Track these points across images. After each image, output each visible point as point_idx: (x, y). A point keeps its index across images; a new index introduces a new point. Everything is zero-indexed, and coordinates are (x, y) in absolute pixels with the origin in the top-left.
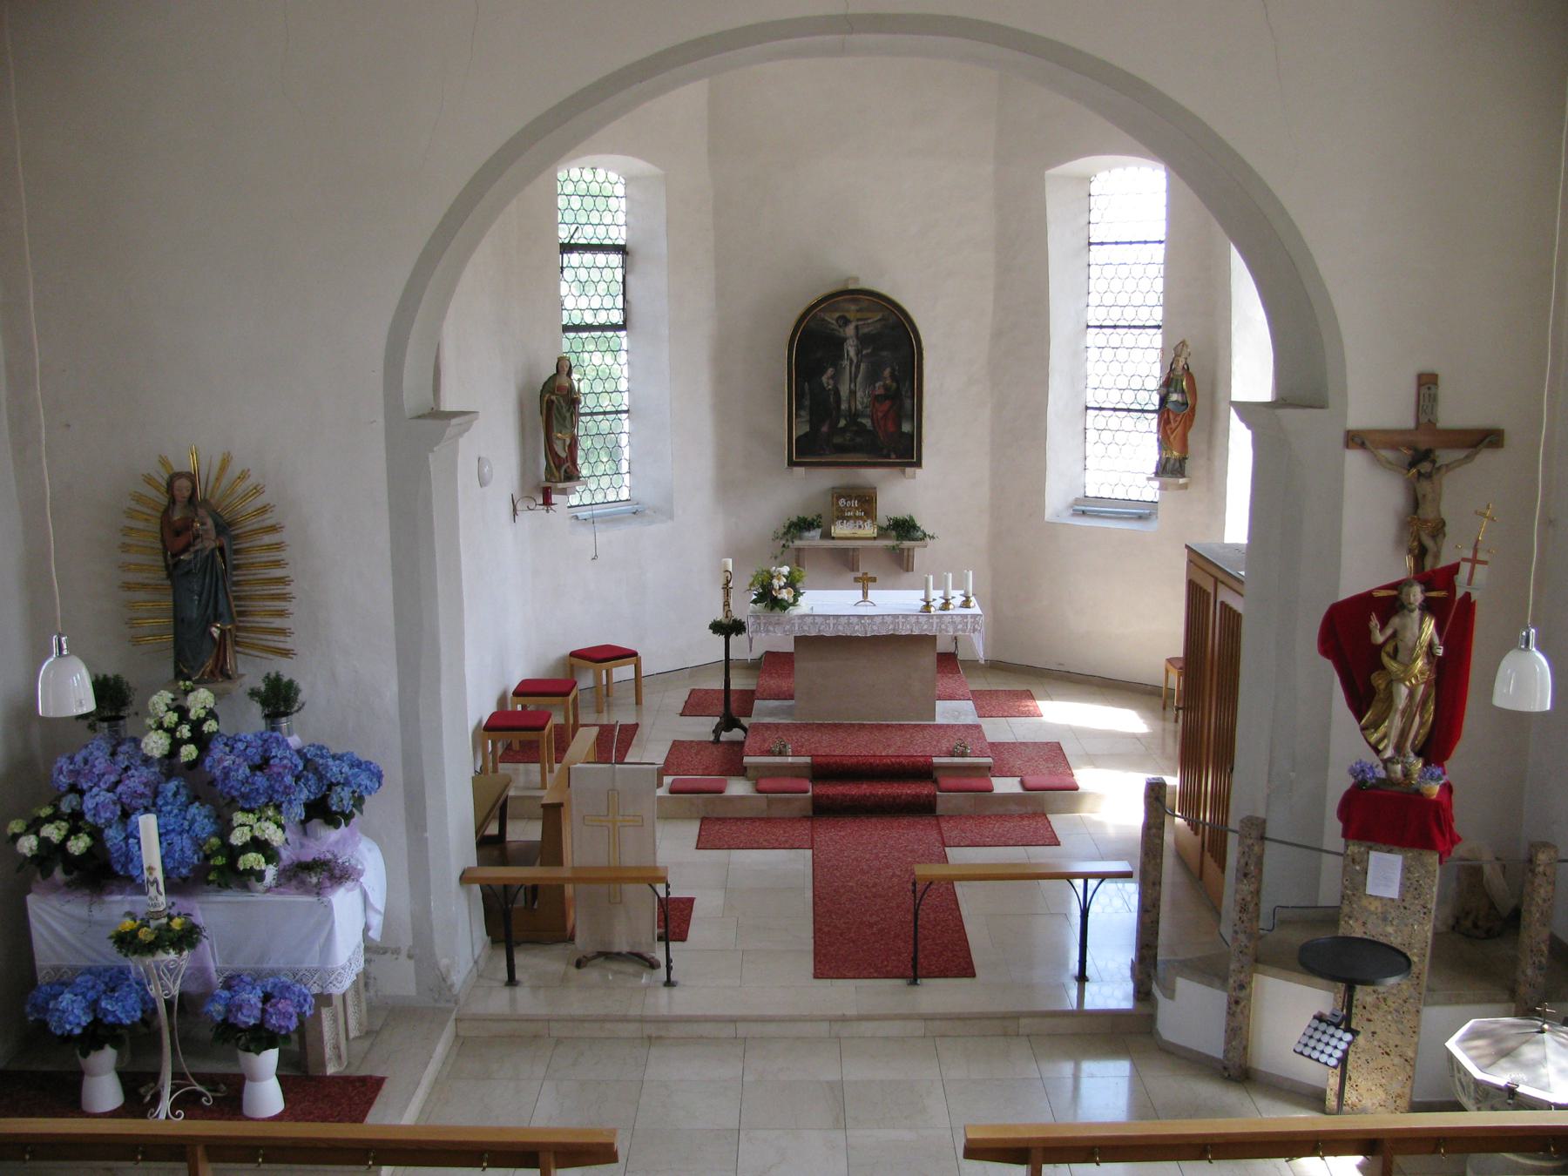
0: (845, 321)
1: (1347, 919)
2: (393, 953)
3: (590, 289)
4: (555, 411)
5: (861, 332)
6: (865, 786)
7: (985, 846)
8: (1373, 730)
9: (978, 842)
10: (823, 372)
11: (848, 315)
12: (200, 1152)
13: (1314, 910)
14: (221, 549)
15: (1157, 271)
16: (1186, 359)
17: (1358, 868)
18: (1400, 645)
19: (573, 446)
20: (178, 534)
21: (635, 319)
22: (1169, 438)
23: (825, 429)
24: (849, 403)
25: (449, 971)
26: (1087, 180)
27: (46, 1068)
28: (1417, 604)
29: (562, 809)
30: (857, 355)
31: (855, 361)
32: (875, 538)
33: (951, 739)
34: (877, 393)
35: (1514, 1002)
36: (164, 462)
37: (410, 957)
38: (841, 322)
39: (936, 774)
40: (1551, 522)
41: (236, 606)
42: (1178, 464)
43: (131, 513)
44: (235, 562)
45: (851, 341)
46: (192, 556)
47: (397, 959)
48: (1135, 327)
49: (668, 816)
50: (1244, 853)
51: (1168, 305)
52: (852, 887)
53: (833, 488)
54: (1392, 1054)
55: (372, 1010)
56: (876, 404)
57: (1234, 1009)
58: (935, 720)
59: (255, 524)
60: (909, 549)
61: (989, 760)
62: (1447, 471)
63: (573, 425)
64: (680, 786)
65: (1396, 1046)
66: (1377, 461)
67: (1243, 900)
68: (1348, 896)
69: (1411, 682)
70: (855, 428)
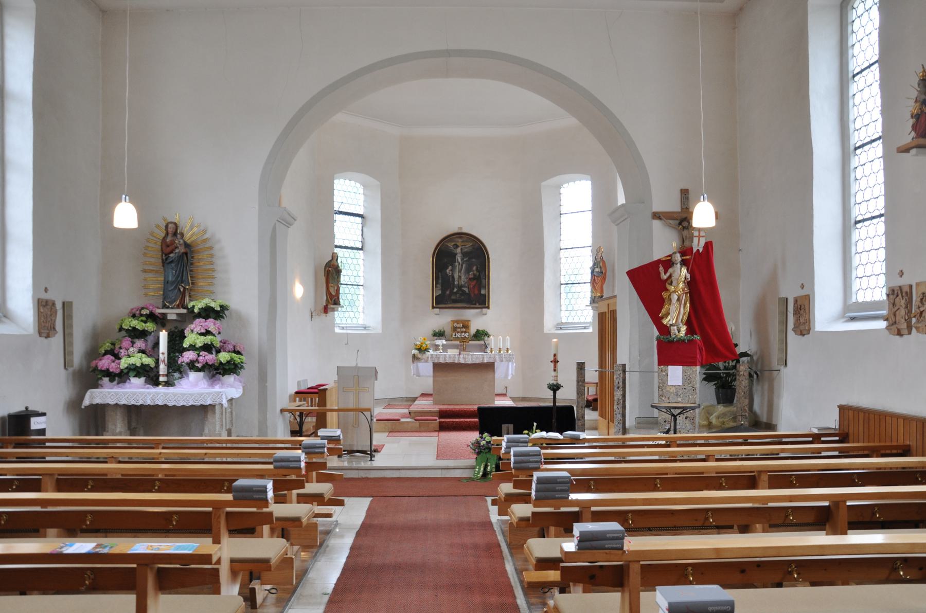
0: (457, 246)
4: (330, 275)
5: (463, 251)
10: (447, 268)
11: (458, 244)
17: (664, 374)
19: (338, 291)
20: (168, 246)
21: (367, 247)
22: (595, 287)
23: (448, 292)
24: (458, 282)
26: (559, 187)
29: (327, 391)
30: (462, 260)
31: (461, 263)
36: (165, 219)
38: (455, 246)
70: (460, 292)
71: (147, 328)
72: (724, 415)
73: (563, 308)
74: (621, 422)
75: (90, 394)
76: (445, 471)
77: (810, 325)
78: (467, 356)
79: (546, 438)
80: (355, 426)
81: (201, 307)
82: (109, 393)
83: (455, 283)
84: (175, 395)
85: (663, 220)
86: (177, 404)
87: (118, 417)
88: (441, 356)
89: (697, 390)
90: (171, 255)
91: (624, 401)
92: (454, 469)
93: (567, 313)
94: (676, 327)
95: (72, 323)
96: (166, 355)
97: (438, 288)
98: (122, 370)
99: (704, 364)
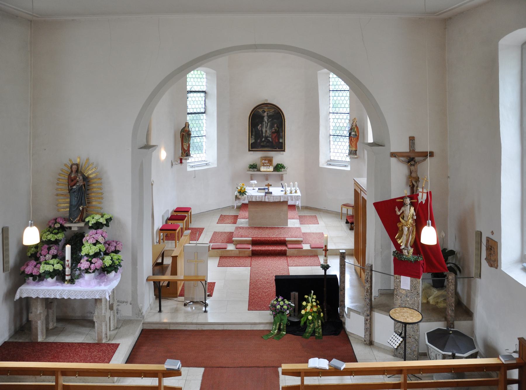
0: (265, 112)
1: (396, 296)
2: (126, 303)
3: (195, 103)
4: (184, 137)
5: (268, 115)
6: (267, 247)
7: (300, 266)
8: (399, 240)
9: (298, 265)
10: (258, 126)
11: (265, 110)
12: (59, 373)
13: (389, 291)
14: (84, 185)
18: (404, 215)
19: (189, 147)
20: (72, 181)
21: (207, 112)
22: (352, 144)
23: (259, 141)
25: (142, 308)
27: (20, 341)
28: (408, 204)
30: (267, 121)
32: (272, 171)
33: (292, 232)
34: (273, 131)
35: (446, 321)
36: (70, 160)
37: (131, 304)
39: (287, 243)
40: (448, 177)
41: (87, 201)
42: (355, 152)
43: (60, 174)
44: (88, 188)
46: (76, 187)
47: (127, 305)
48: (343, 113)
49: (211, 256)
52: (261, 280)
53: (261, 157)
54: (412, 338)
55: (118, 321)
56: (273, 134)
57: (367, 322)
58: (288, 226)
60: (282, 175)
61: (302, 239)
62: (419, 163)
63: (189, 141)
64: (215, 247)
65: (413, 335)
66: (399, 160)
68: (396, 289)
69: (408, 226)
70: (267, 141)
71: (58, 238)
72: (438, 297)
73: (332, 150)
74: (369, 304)
75: (20, 290)
76: (253, 326)
77: (498, 263)
78: (270, 197)
79: (318, 368)
80: (195, 285)
81: (93, 223)
82: (32, 290)
83: (263, 135)
84: (75, 291)
85: (397, 157)
86: (76, 298)
87: (38, 303)
88: (254, 197)
89: (420, 295)
90: (74, 187)
91: (371, 290)
92: (259, 324)
94: (406, 251)
95: (8, 242)
96: (70, 262)
97: (253, 138)
98: (41, 273)
99: (424, 272)
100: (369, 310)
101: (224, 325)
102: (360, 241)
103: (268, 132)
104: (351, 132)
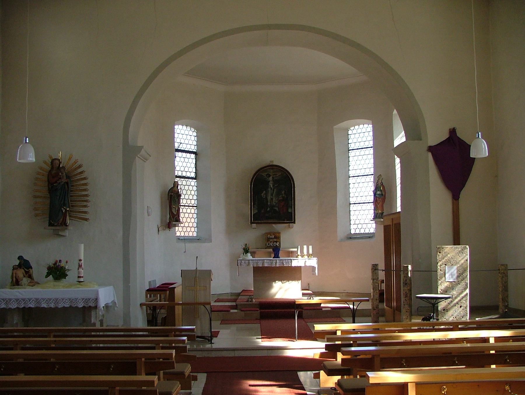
0: (269, 176)
15: (371, 157)
16: (382, 180)
24: (271, 203)
26: (347, 130)
30: (273, 186)
31: (272, 189)
36: (50, 157)
43: (38, 173)
45: (271, 183)
48: (365, 175)
50: (405, 276)
51: (375, 167)
59: (78, 177)
67: (406, 293)
73: (352, 222)
83: (269, 204)
93: (355, 226)
97: (255, 208)
100: (409, 317)
101: (236, 351)
102: (393, 288)
103: (274, 200)
104: (376, 193)
